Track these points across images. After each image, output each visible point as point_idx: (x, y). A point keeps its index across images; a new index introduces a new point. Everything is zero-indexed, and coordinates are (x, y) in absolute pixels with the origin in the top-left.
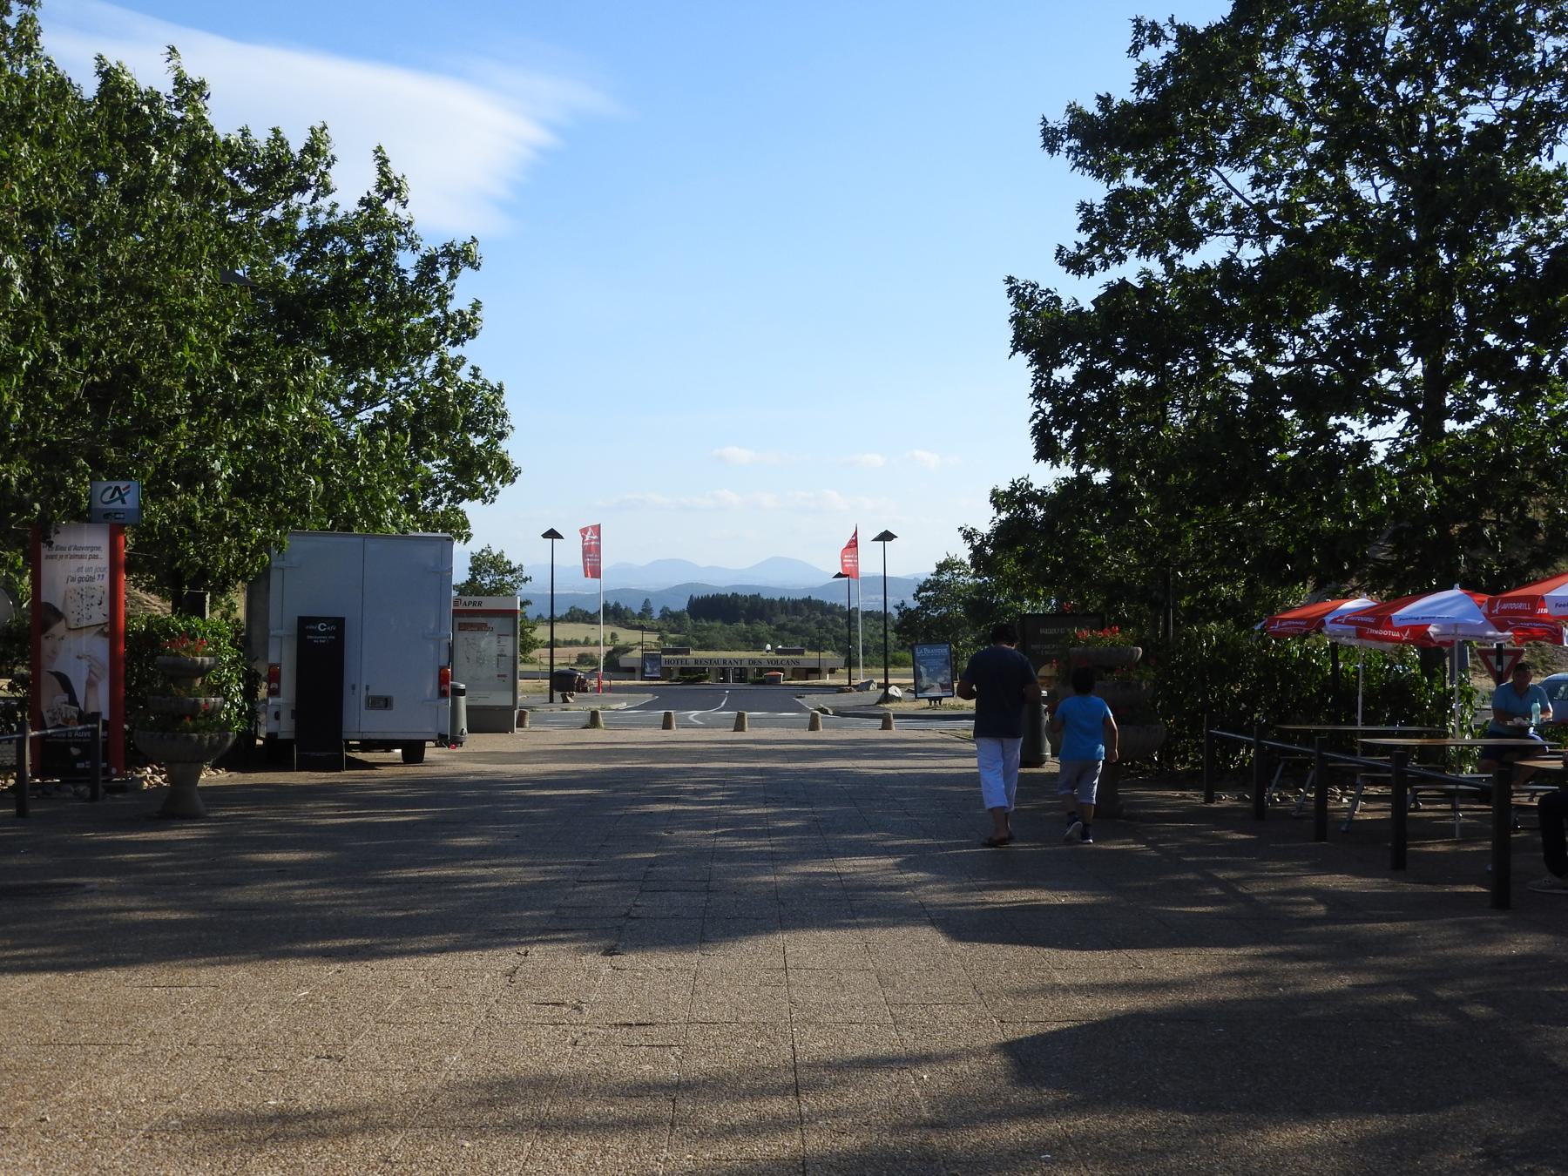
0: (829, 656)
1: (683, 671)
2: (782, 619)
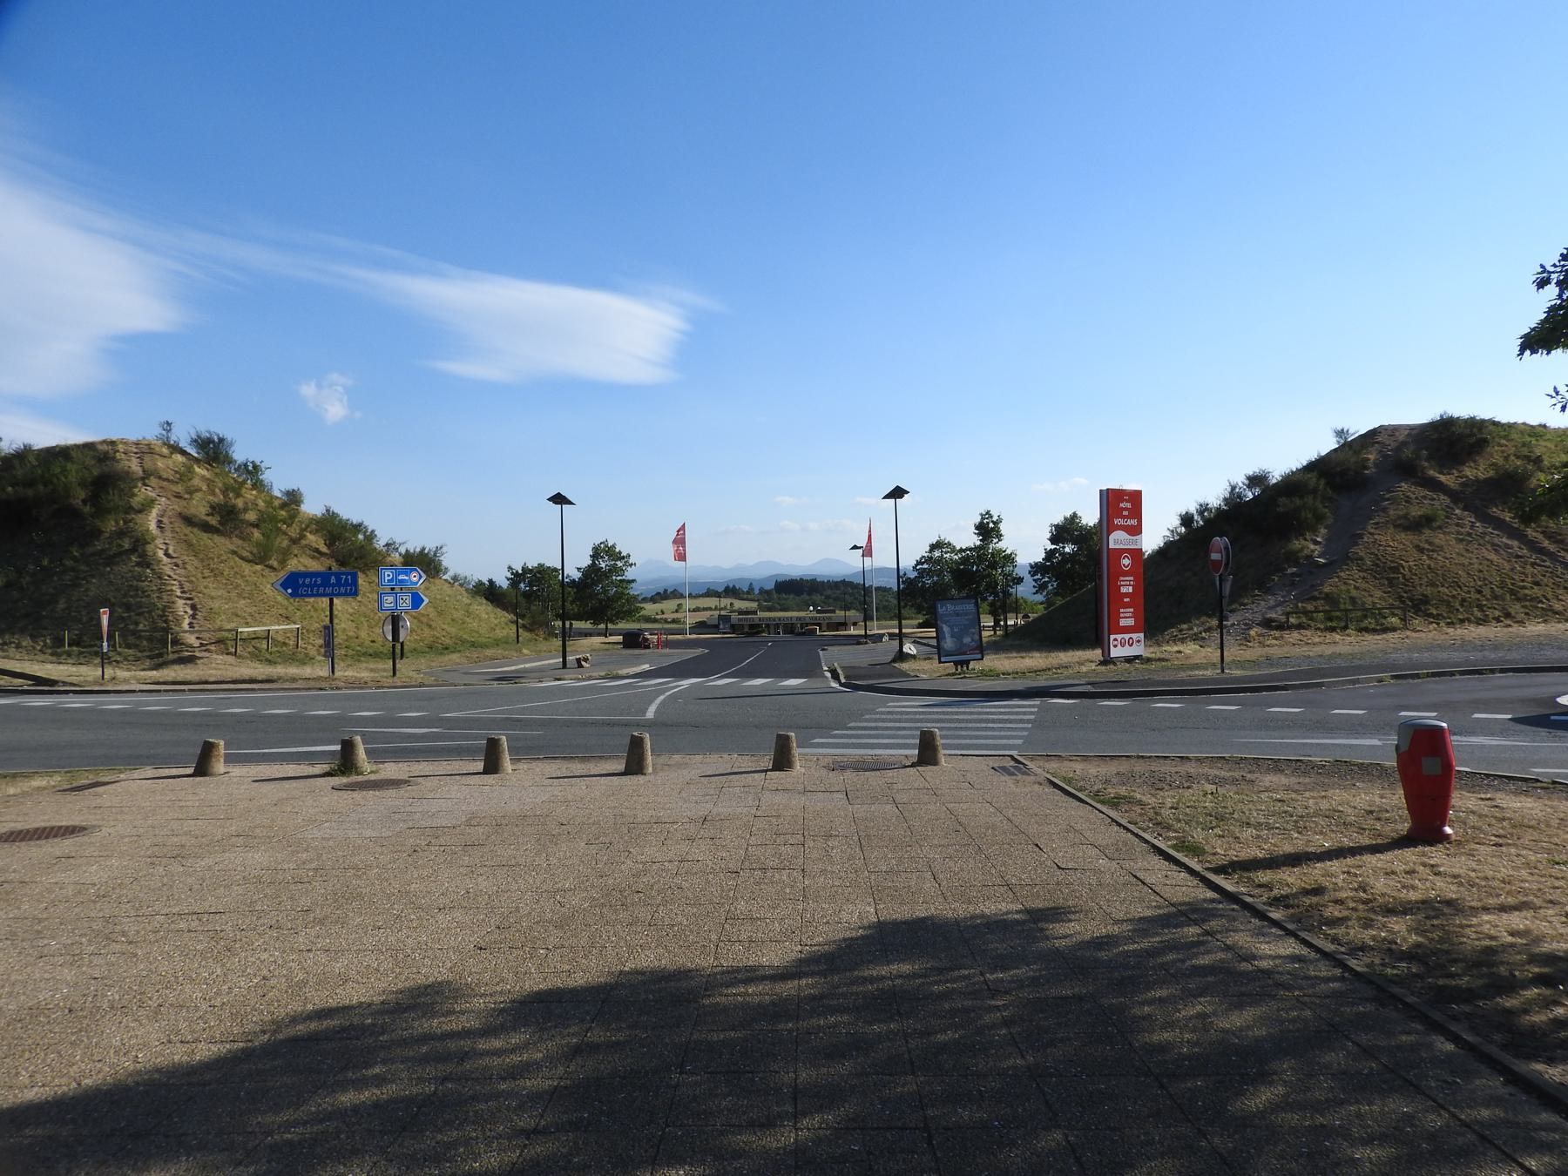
0: (852, 613)
1: (752, 626)
2: (829, 592)
